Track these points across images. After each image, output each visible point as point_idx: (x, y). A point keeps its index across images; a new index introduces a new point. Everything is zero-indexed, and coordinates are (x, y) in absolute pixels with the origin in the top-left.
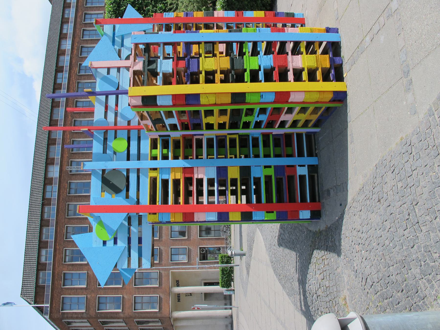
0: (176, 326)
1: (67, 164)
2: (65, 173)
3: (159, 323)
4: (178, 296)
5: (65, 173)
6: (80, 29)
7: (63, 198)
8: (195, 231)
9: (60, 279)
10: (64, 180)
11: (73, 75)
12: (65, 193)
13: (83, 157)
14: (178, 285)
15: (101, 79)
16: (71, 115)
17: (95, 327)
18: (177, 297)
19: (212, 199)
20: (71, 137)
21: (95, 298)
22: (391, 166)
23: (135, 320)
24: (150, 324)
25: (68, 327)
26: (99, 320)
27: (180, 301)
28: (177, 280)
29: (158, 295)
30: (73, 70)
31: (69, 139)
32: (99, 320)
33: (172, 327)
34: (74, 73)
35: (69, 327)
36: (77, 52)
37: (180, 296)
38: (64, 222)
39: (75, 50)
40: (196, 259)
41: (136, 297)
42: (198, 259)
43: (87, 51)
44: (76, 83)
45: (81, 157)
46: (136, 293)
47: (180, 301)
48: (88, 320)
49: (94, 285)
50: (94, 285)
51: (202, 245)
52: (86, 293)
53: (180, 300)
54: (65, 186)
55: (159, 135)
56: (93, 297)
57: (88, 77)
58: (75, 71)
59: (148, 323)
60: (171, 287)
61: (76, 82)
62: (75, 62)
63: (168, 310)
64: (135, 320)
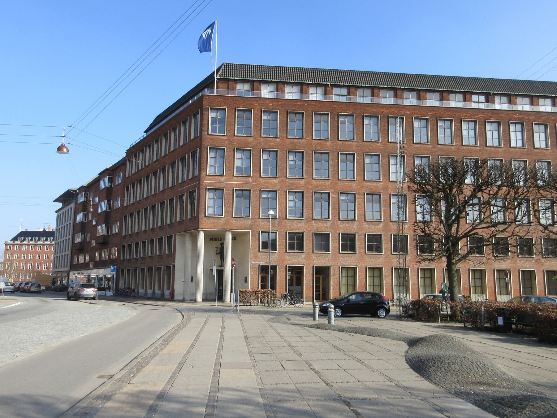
0: (185, 235)
1: (375, 112)
2: (364, 110)
3: (190, 216)
4: (216, 238)
5: (364, 110)
6: (547, 121)
7: (335, 108)
8: (295, 261)
9: (245, 106)
10: (356, 109)
11: (485, 115)
12: (341, 110)
13: (383, 130)
14: (234, 239)
15: (494, 103)
16: (434, 115)
17: (188, 144)
18: (215, 237)
19: (332, 283)
20: (407, 115)
21: (223, 145)
22: (411, 392)
23: (196, 189)
24: (189, 206)
25: (191, 115)
26: (198, 149)
27: (210, 240)
28: (236, 238)
29: (223, 216)
30: (492, 115)
31: (405, 113)
32: (198, 149)
33: (184, 230)
34: (488, 116)
35: (190, 116)
36: (515, 118)
37: (216, 240)
38: (308, 110)
39: (518, 115)
40: (263, 261)
41: (222, 191)
42: (262, 263)
43: (426, 277)
44: (475, 119)
45: (382, 128)
46: (227, 191)
47: (210, 240)
48: (199, 137)
49: (237, 143)
50: (237, 143)
51: (279, 269)
52: (228, 135)
53: (211, 241)
54: (349, 110)
55: (144, 132)
56: (224, 143)
57: (482, 133)
58: (490, 117)
59: (190, 204)
60: (204, 230)
61: (476, 119)
62: (501, 116)
63: (207, 227)
64: (196, 189)
